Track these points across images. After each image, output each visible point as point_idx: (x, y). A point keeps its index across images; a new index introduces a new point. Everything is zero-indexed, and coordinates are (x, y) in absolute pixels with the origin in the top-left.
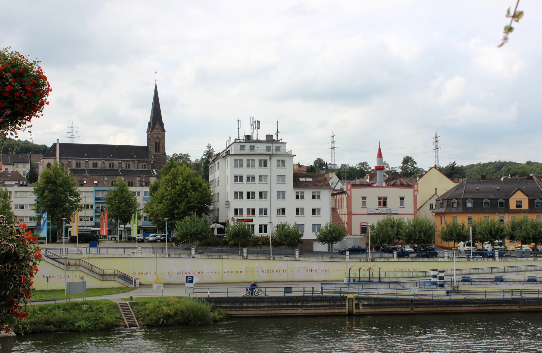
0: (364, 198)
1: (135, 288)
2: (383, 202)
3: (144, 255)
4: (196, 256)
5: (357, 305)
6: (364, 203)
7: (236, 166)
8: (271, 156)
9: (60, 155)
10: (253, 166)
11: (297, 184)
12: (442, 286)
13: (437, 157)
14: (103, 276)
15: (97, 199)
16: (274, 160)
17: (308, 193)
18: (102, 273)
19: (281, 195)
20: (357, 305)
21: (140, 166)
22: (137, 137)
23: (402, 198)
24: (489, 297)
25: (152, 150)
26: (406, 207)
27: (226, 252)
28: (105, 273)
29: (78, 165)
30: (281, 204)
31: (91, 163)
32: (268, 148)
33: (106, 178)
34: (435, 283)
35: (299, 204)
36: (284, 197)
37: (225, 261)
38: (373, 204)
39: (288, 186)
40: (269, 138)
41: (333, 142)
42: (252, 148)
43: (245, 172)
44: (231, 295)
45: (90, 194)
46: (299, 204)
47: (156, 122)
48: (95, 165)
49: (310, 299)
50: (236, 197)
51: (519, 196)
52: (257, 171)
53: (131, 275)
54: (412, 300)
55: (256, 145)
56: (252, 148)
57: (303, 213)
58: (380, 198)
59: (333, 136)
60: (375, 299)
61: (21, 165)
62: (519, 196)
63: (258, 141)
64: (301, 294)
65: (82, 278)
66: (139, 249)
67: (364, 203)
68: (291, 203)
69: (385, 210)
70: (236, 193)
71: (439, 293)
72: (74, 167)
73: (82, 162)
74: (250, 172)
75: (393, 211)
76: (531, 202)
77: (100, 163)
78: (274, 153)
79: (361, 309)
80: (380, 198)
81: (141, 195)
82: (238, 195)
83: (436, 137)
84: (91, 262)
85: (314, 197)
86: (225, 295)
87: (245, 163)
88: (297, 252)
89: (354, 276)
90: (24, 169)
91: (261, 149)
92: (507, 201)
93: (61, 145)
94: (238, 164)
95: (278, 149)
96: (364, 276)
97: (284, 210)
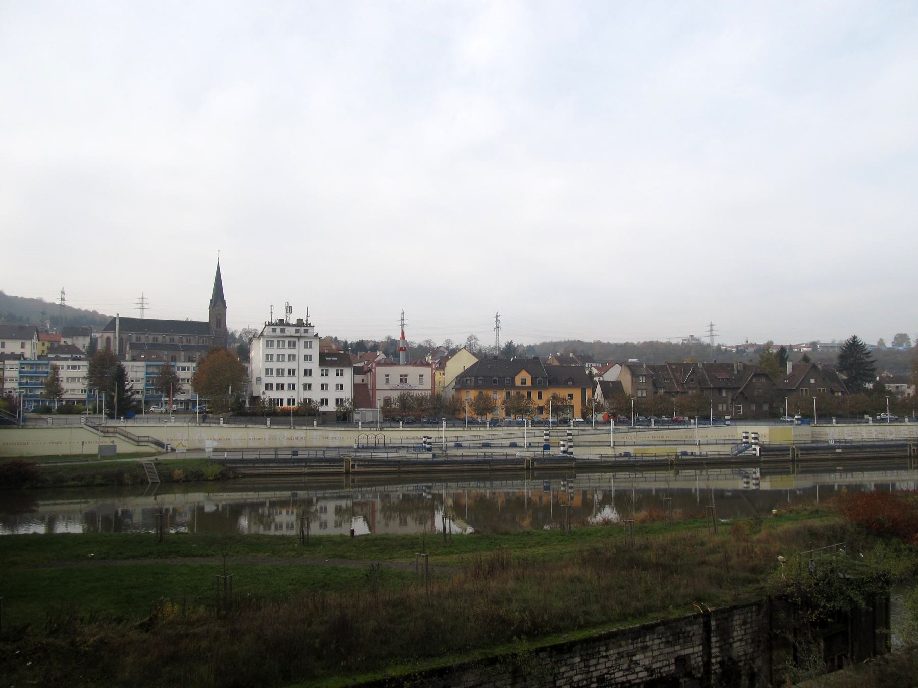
0: (387, 375)
1: (167, 452)
2: (404, 378)
3: (177, 424)
4: (225, 425)
5: (353, 466)
6: (387, 380)
7: (267, 346)
8: (299, 338)
9: (120, 330)
10: (272, 346)
11: (323, 362)
12: (430, 450)
13: (497, 335)
14: (138, 442)
15: (147, 373)
16: (302, 342)
17: (332, 371)
18: (136, 439)
19: (308, 372)
20: (353, 466)
21: (201, 341)
22: (202, 314)
23: (421, 376)
24: (465, 458)
25: (214, 326)
26: (421, 381)
27: (253, 423)
28: (140, 439)
29: (138, 339)
30: (308, 380)
31: (151, 337)
32: (297, 331)
33: (166, 352)
34: (425, 448)
35: (325, 380)
36: (310, 374)
37: (203, 429)
38: (395, 381)
39: (314, 365)
40: (300, 323)
41: (403, 319)
42: (283, 331)
43: (275, 351)
44: (245, 457)
45: (141, 369)
46: (325, 380)
47: (218, 301)
48: (155, 339)
49: (99, 480)
50: (267, 374)
51: (524, 374)
52: (287, 351)
53: (165, 442)
54: (399, 462)
55: (287, 328)
56: (283, 331)
57: (327, 389)
58: (401, 376)
59: (403, 314)
60: (369, 461)
61: (80, 339)
62: (524, 374)
63: (288, 324)
64: (306, 456)
65: (113, 442)
66: (173, 419)
67: (387, 380)
68: (316, 379)
69: (406, 387)
70: (267, 370)
71: (428, 455)
72: (134, 341)
73: (142, 337)
74: (281, 351)
75: (413, 387)
76: (534, 379)
77: (160, 338)
78: (303, 335)
79: (357, 469)
80: (401, 376)
81: (186, 371)
82: (269, 372)
83: (497, 316)
84: (128, 430)
85: (337, 374)
86: (240, 457)
87: (275, 344)
88: (315, 422)
89: (363, 443)
90: (82, 343)
91: (291, 331)
92: (513, 379)
93: (122, 320)
94: (269, 344)
95: (306, 331)
96: (372, 443)
97: (310, 386)
